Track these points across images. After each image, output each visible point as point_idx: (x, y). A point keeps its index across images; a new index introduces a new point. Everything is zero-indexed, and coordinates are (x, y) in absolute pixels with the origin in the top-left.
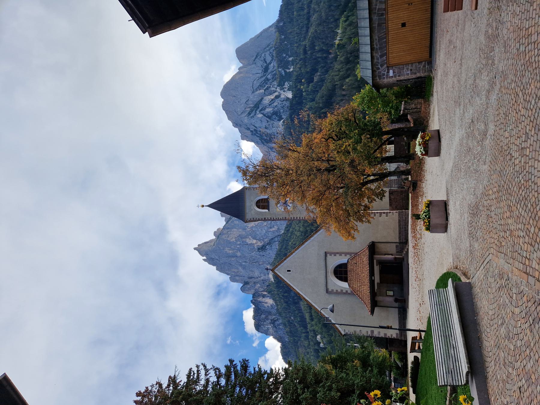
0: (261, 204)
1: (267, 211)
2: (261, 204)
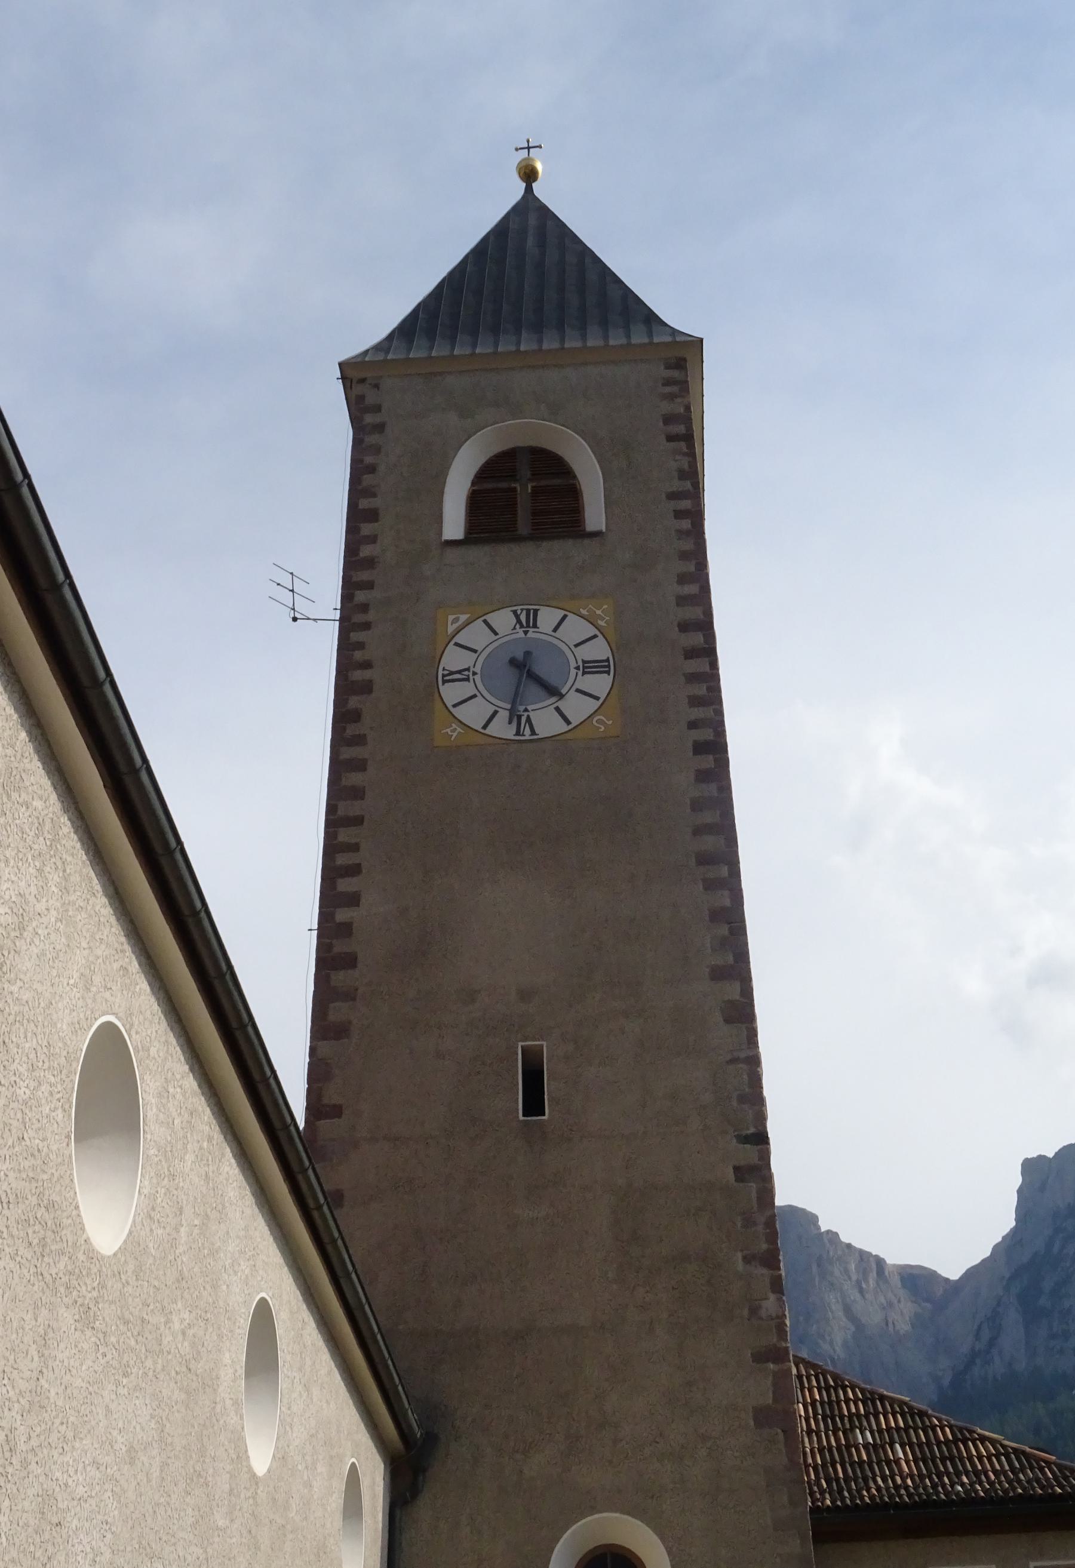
0: (524, 489)
1: (454, 525)
2: (524, 489)
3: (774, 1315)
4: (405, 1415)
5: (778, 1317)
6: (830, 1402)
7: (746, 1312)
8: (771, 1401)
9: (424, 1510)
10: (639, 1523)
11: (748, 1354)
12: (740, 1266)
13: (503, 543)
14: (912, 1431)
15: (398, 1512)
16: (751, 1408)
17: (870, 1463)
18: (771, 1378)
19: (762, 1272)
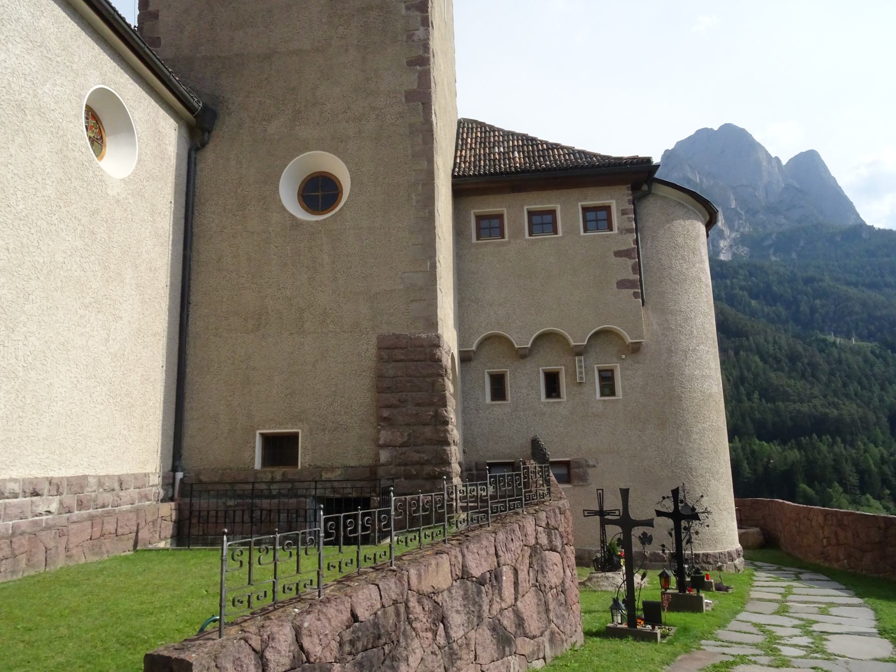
3: (422, 38)
4: (170, 80)
5: (425, 40)
6: (485, 138)
7: (405, 38)
8: (416, 87)
9: (209, 156)
10: (333, 155)
11: (404, 61)
12: (404, 12)
13: (680, 398)
14: (525, 147)
15: (193, 153)
16: (404, 92)
17: (499, 160)
18: (417, 74)
19: (418, 14)
